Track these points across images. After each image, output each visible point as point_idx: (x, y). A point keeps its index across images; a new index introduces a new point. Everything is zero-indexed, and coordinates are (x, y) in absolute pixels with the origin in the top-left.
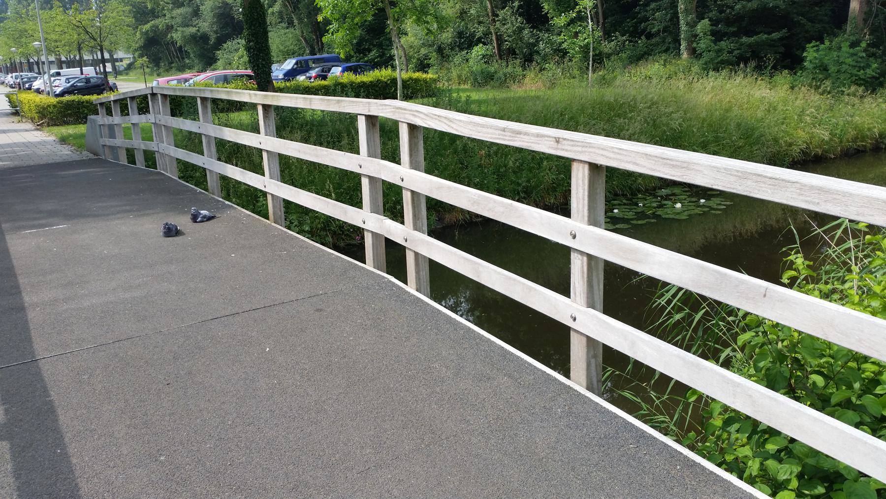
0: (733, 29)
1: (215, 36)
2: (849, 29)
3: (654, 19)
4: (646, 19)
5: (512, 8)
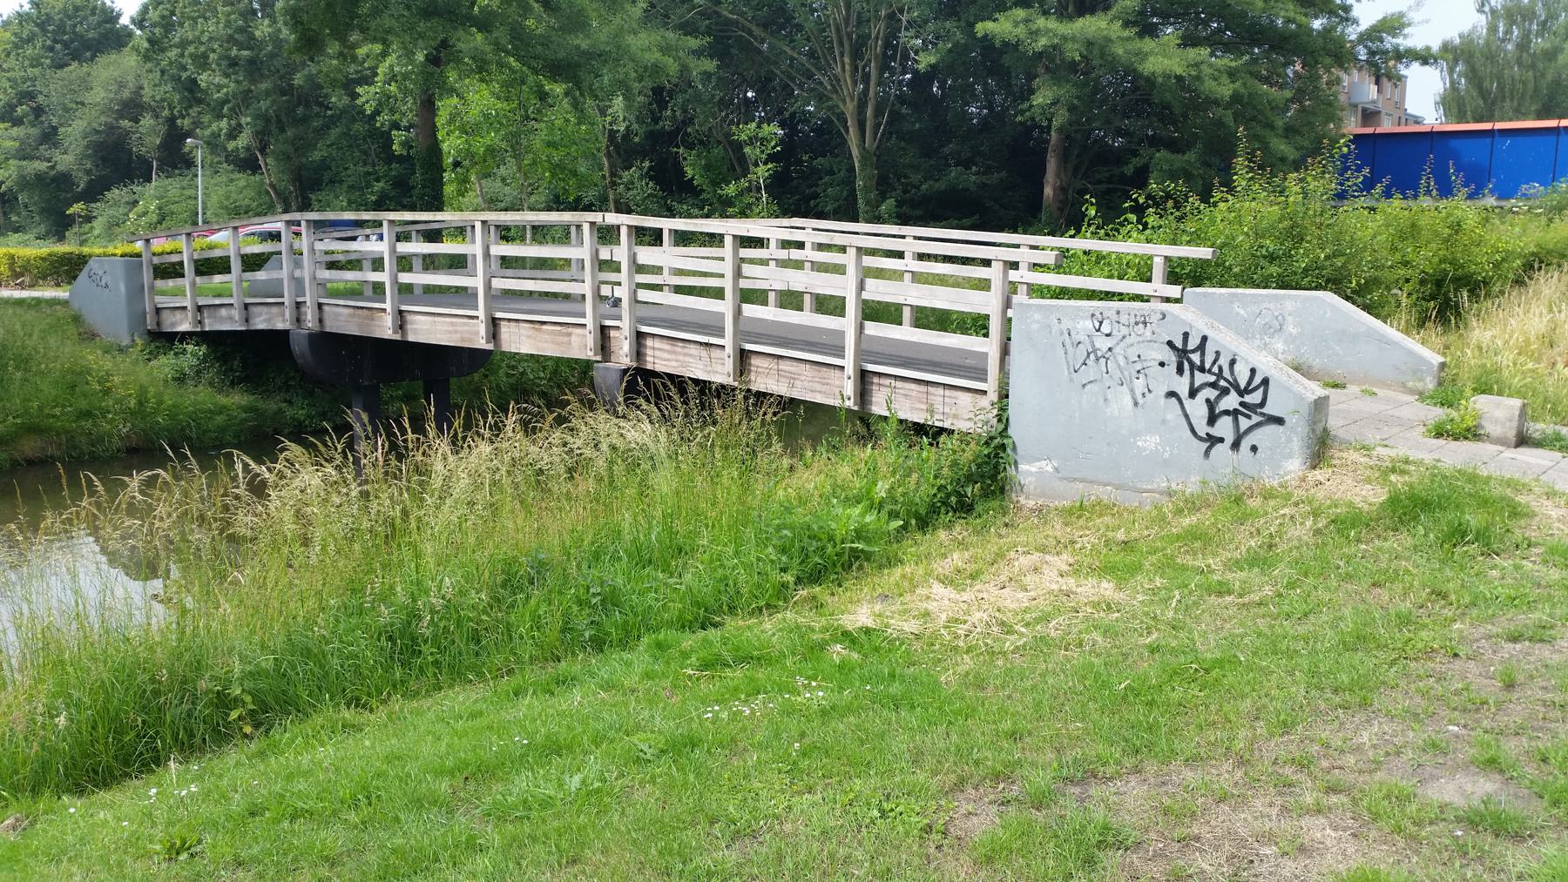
0: (919, 213)
1: (86, 178)
2: (1043, 218)
3: (826, 196)
4: (816, 196)
5: (641, 169)
